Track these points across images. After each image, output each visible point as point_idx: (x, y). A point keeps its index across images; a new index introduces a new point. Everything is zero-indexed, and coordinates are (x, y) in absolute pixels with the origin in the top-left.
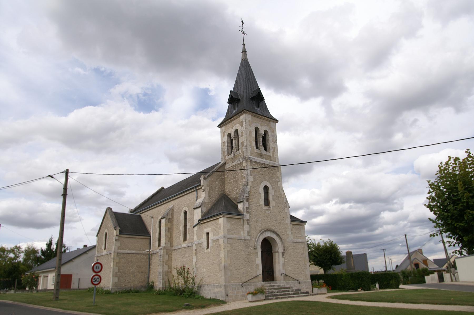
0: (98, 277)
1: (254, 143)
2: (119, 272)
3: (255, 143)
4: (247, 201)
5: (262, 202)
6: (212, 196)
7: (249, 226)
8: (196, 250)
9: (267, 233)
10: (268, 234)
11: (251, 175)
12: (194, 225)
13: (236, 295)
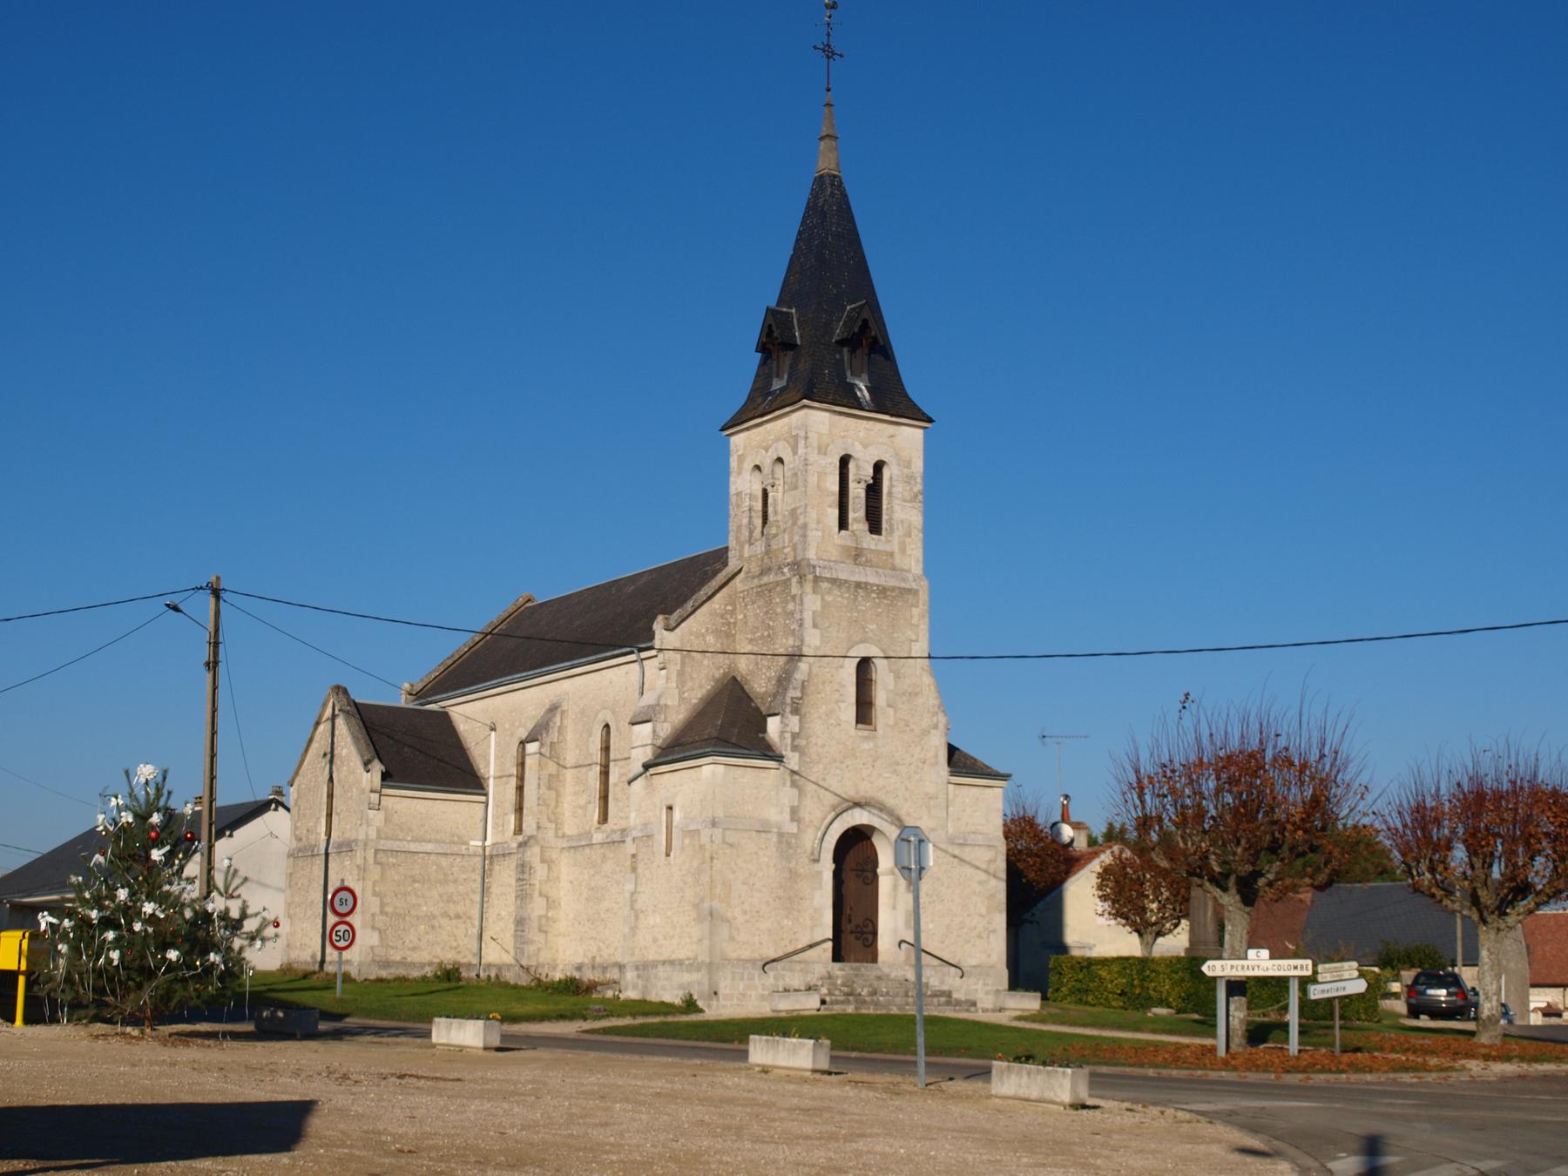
2: (382, 912)
3: (836, 512)
4: (796, 711)
5: (849, 711)
6: (690, 684)
7: (795, 791)
8: (634, 856)
9: (857, 811)
10: (859, 817)
11: (815, 626)
12: (631, 775)
13: (744, 995)
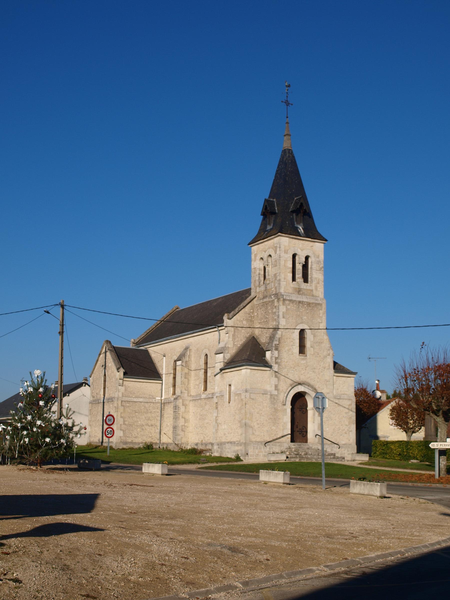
0: (111, 430)
1: (291, 275)
2: (124, 424)
3: (291, 275)
4: (277, 349)
7: (276, 379)
8: (217, 403)
9: (300, 386)
11: (283, 317)
12: (215, 373)
13: (258, 455)
